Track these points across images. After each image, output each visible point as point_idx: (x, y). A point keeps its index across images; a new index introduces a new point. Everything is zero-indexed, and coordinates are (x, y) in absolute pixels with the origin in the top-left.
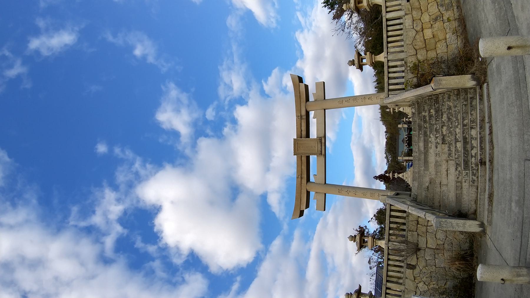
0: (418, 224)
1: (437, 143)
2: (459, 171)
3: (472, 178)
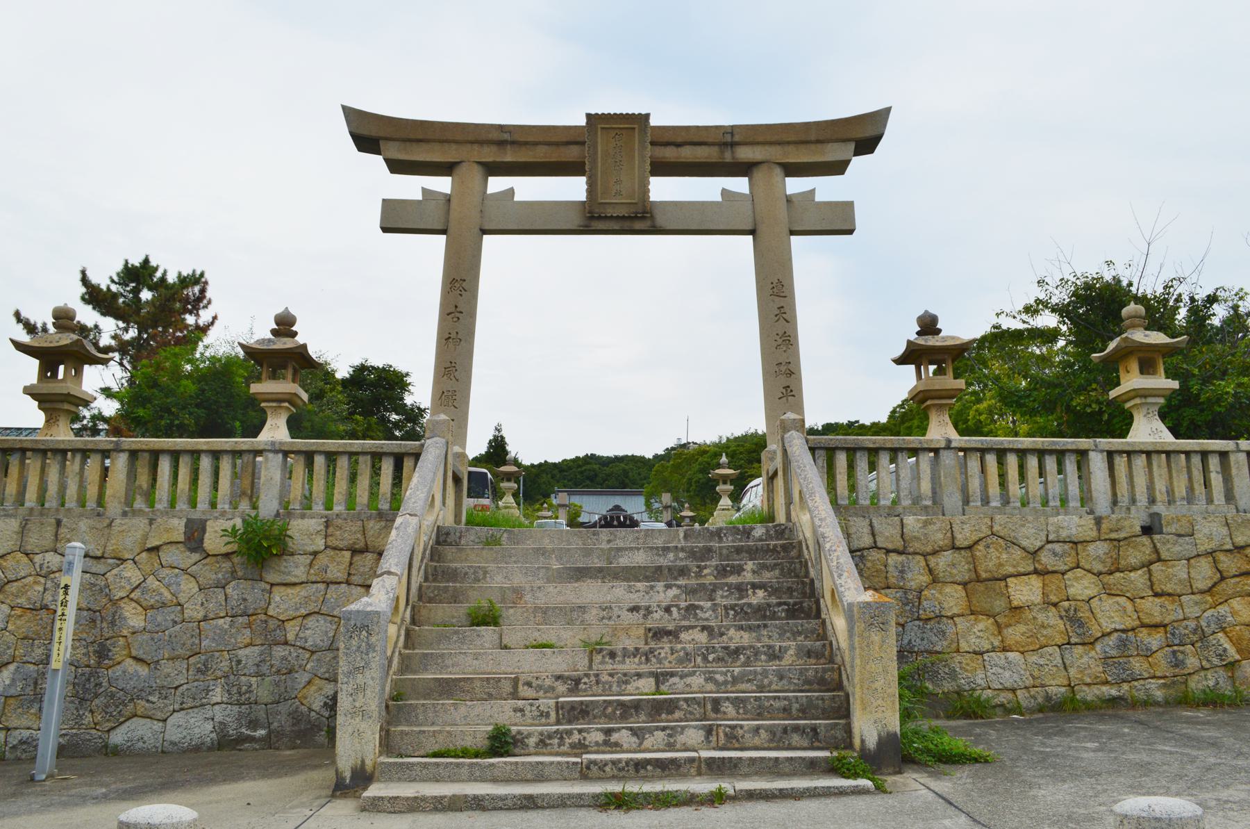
0: (355, 552)
1: (649, 611)
2: (553, 689)
3: (529, 735)
